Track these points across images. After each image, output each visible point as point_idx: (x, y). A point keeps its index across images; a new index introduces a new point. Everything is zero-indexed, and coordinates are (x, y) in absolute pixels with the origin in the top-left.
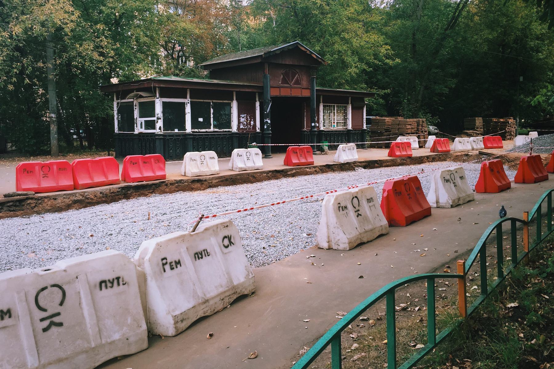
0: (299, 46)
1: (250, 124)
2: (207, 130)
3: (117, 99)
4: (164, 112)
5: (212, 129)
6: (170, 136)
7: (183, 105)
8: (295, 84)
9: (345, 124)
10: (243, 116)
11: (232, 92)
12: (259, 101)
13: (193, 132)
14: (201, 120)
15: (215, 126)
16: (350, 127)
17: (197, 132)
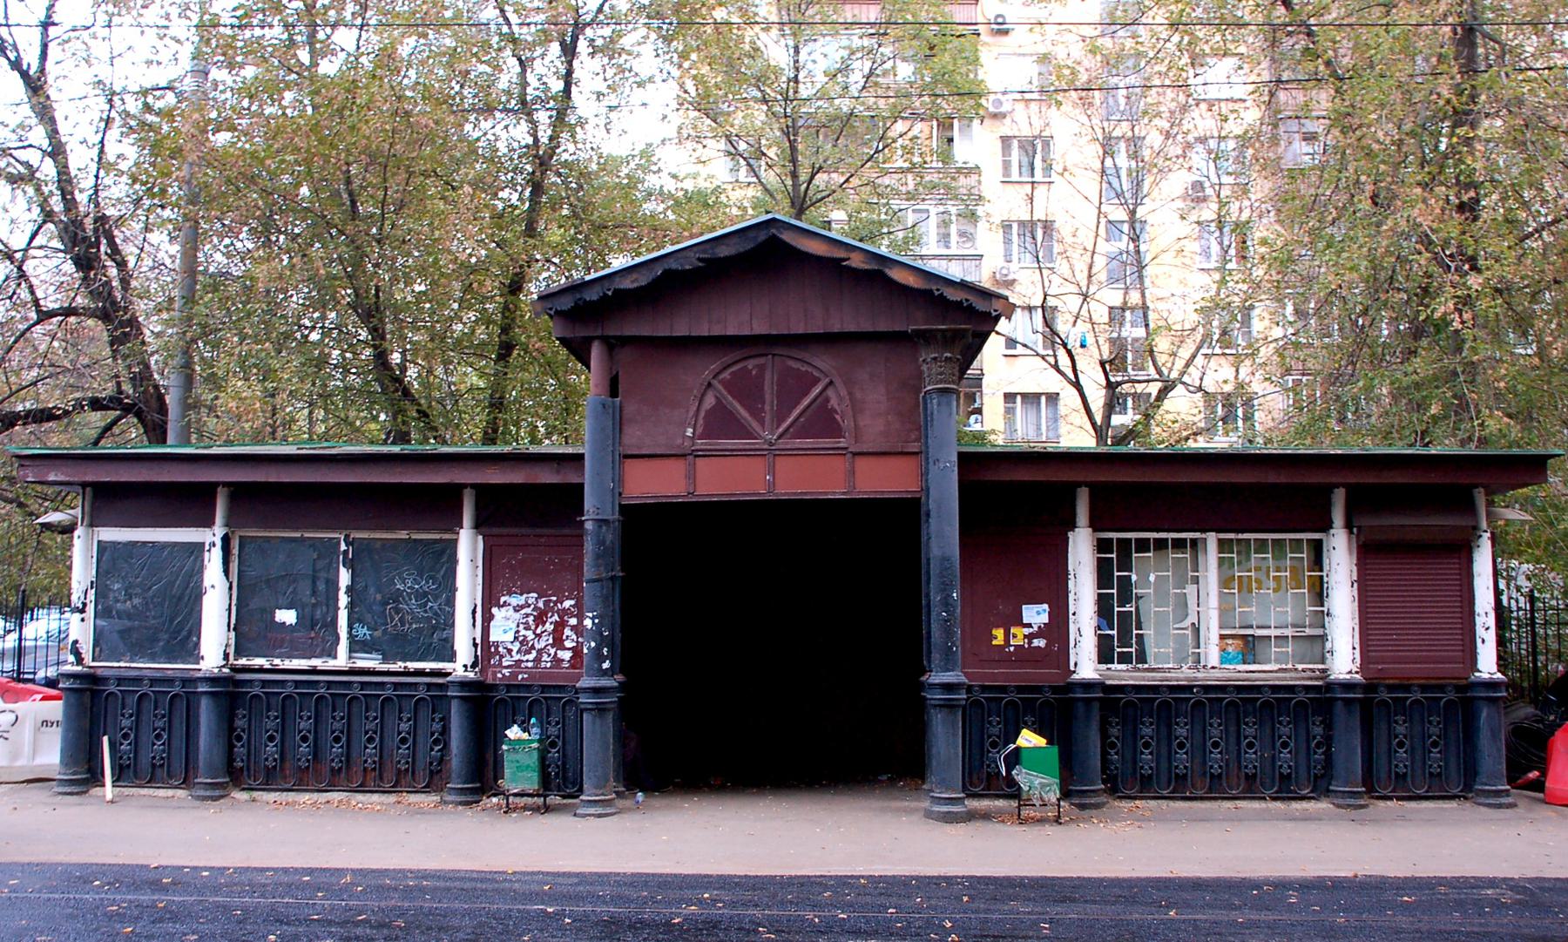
0: (786, 236)
2: (317, 663)
3: (1095, 525)
4: (100, 585)
5: (341, 660)
6: (120, 680)
7: (196, 551)
9: (1317, 643)
12: (1349, 526)
13: (235, 669)
15: (356, 646)
16: (1344, 661)
17: (261, 670)
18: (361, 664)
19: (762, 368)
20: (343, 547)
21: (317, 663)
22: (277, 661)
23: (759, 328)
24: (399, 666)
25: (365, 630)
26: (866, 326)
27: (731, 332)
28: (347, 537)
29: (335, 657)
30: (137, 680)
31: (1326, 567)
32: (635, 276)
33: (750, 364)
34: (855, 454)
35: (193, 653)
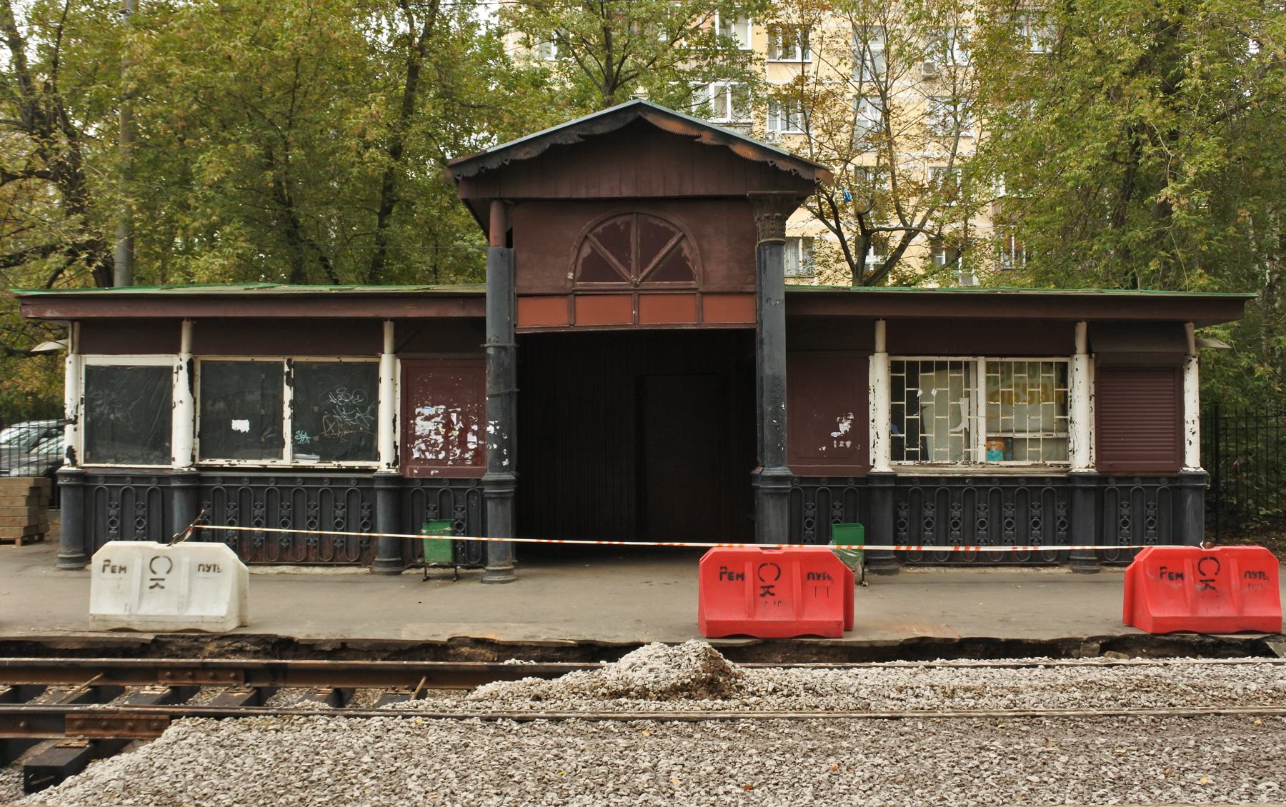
0: (650, 118)
1: (463, 443)
2: (267, 462)
4: (88, 402)
5: (287, 460)
6: (108, 478)
7: (167, 372)
8: (659, 274)
9: (1062, 443)
10: (428, 411)
11: (377, 324)
12: (1089, 352)
14: (241, 425)
15: (299, 448)
16: (1082, 459)
17: (222, 469)
18: (303, 463)
19: (628, 224)
20: (286, 369)
21: (267, 462)
22: (234, 462)
23: (627, 192)
24: (333, 464)
25: (305, 436)
26: (713, 190)
27: (605, 193)
28: (289, 361)
29: (281, 458)
30: (121, 478)
31: (1070, 385)
32: (527, 149)
33: (619, 221)
34: (703, 294)
35: (167, 456)
